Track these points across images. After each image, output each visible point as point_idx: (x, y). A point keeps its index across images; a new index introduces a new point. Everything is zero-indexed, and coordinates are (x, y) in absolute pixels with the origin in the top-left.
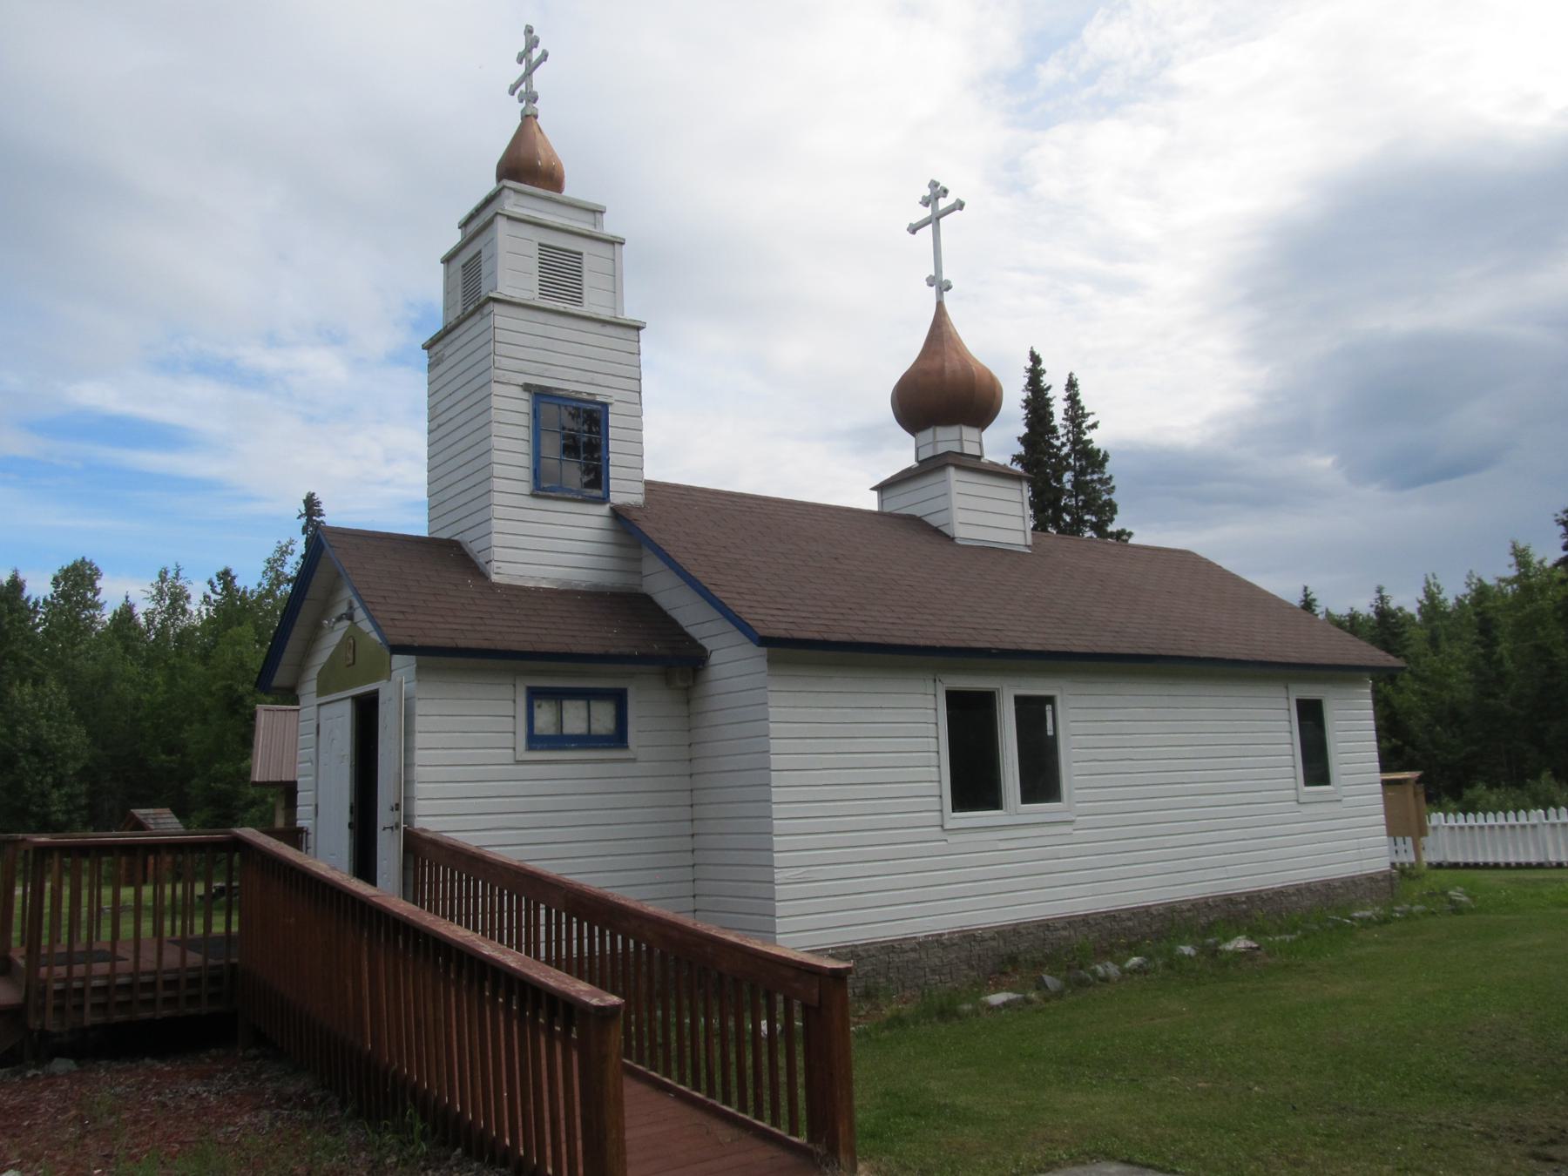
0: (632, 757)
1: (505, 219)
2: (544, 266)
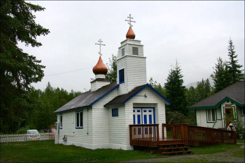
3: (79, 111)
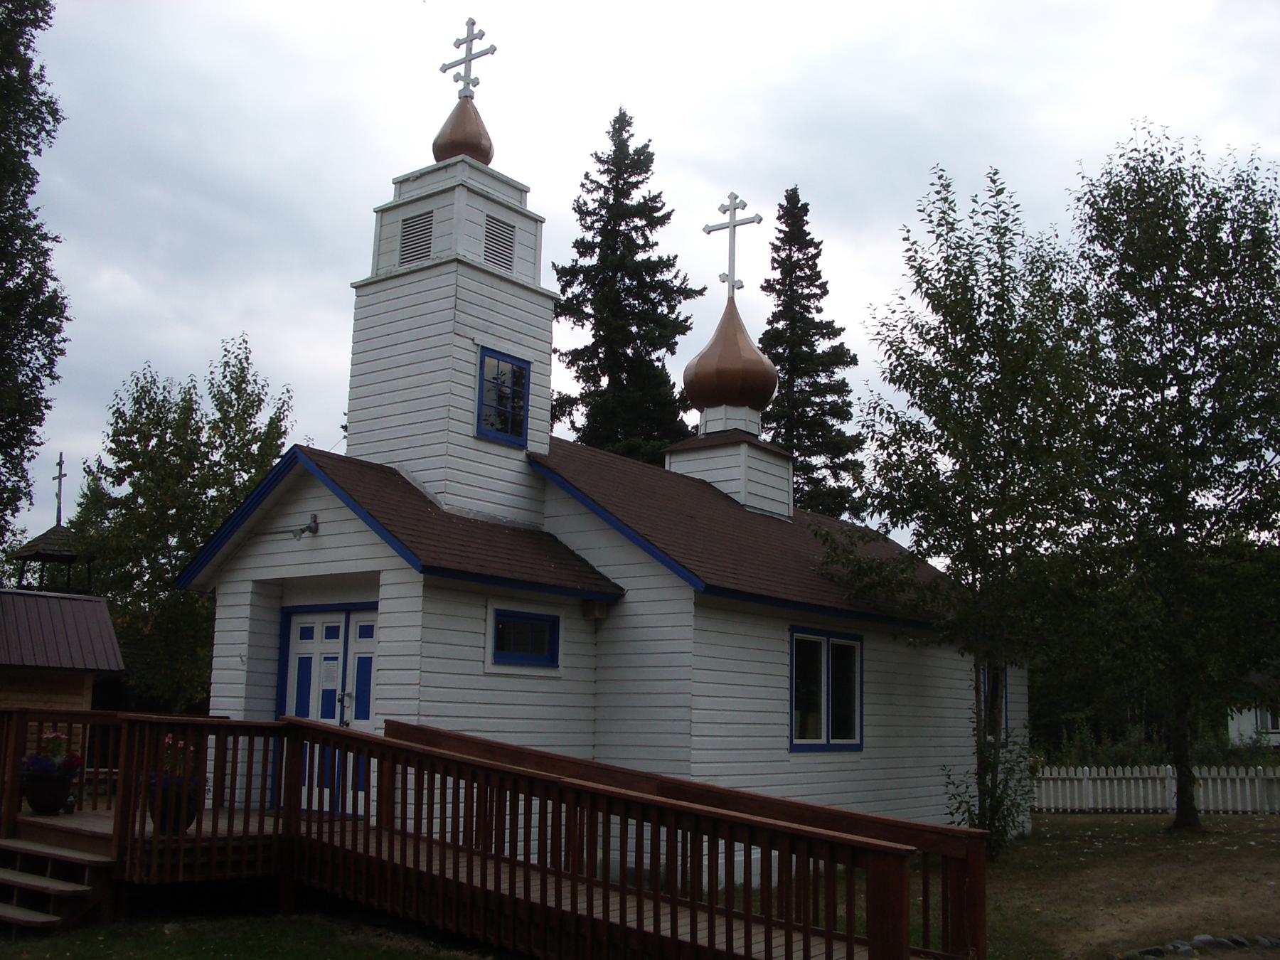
0: (559, 676)
1: (466, 190)
2: (490, 236)
3: (828, 634)
